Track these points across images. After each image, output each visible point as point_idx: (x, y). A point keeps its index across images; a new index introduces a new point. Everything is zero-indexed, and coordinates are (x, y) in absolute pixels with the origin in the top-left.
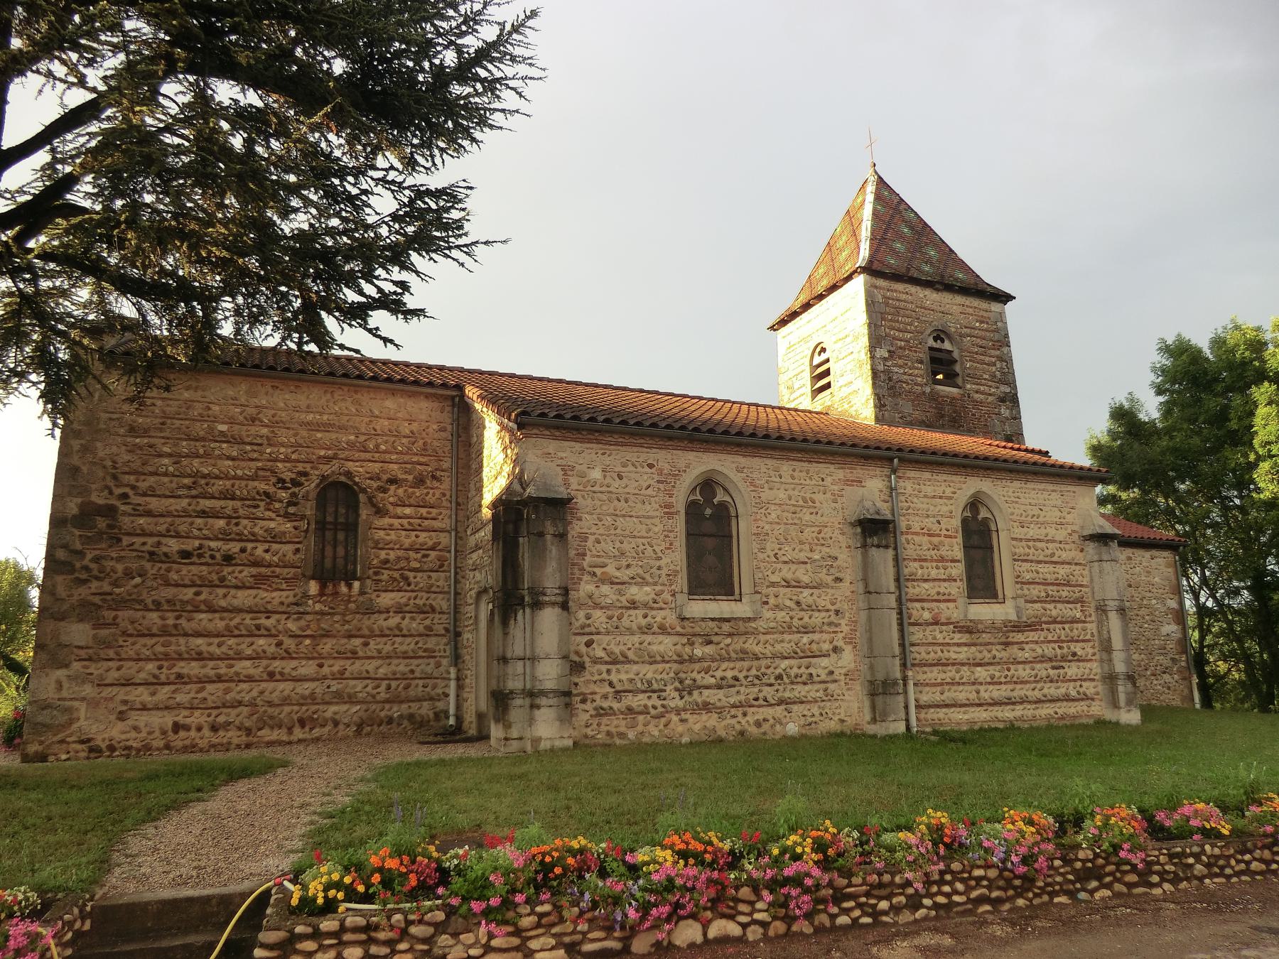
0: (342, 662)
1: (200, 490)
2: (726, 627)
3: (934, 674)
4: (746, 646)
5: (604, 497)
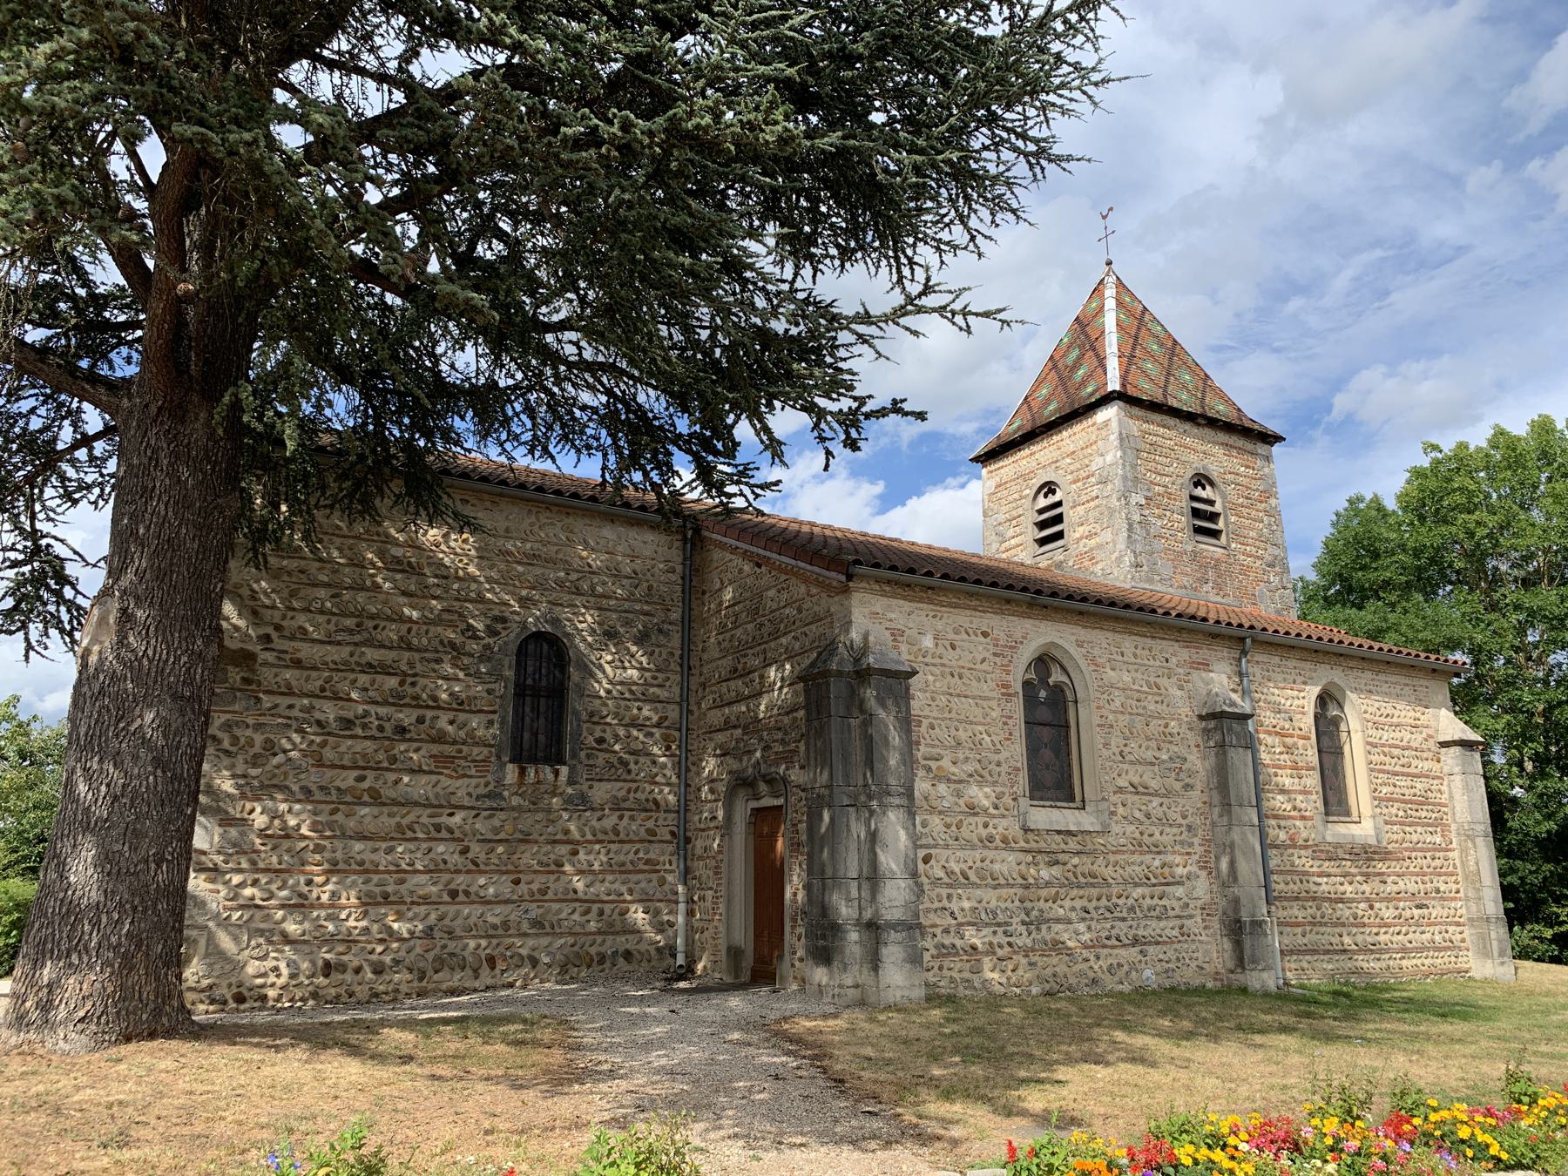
0: (543, 878)
1: (366, 635)
2: (1073, 845)
3: (1296, 912)
4: (1095, 867)
5: (937, 671)
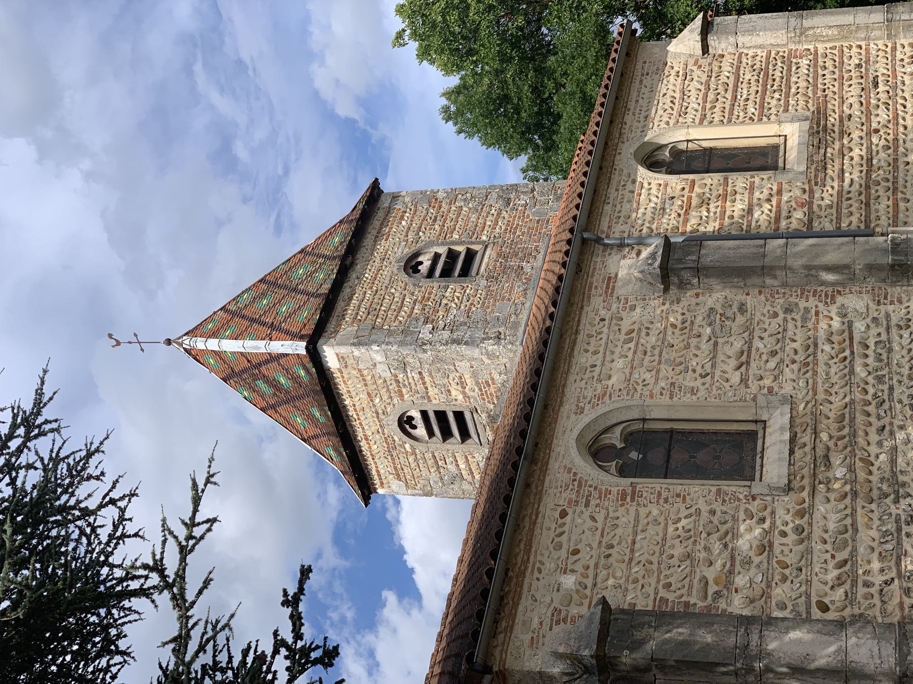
2: (806, 438)
